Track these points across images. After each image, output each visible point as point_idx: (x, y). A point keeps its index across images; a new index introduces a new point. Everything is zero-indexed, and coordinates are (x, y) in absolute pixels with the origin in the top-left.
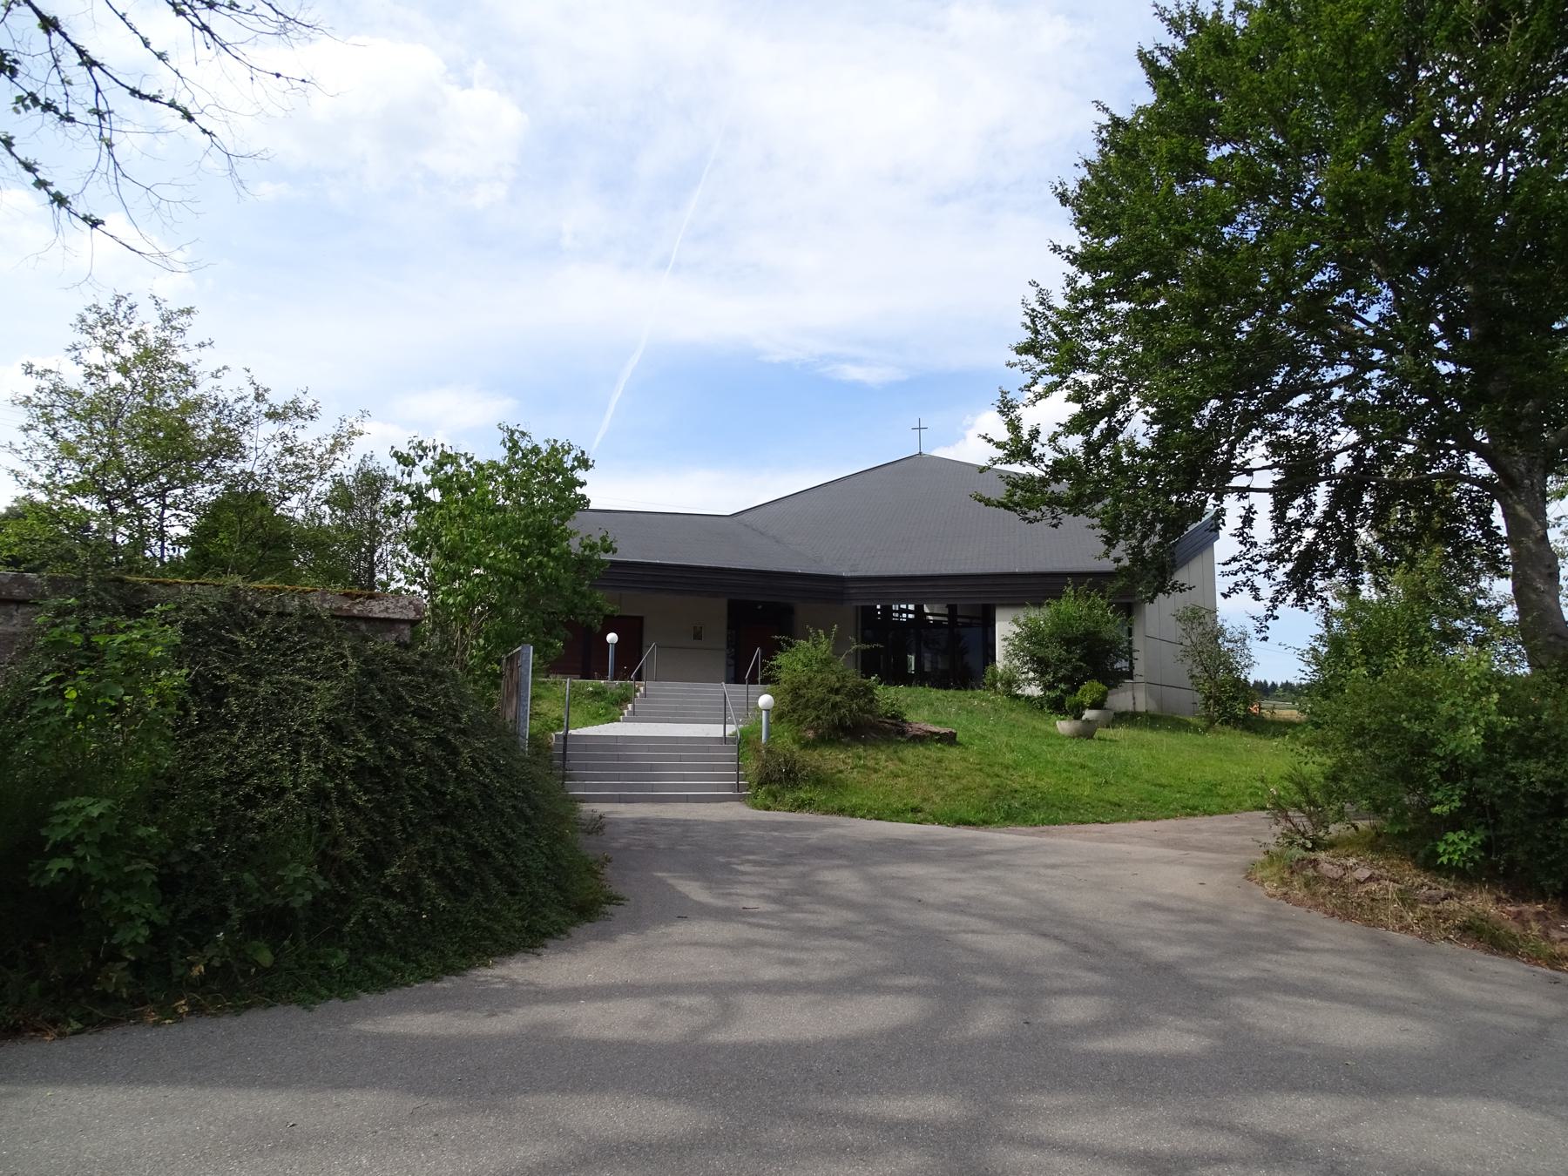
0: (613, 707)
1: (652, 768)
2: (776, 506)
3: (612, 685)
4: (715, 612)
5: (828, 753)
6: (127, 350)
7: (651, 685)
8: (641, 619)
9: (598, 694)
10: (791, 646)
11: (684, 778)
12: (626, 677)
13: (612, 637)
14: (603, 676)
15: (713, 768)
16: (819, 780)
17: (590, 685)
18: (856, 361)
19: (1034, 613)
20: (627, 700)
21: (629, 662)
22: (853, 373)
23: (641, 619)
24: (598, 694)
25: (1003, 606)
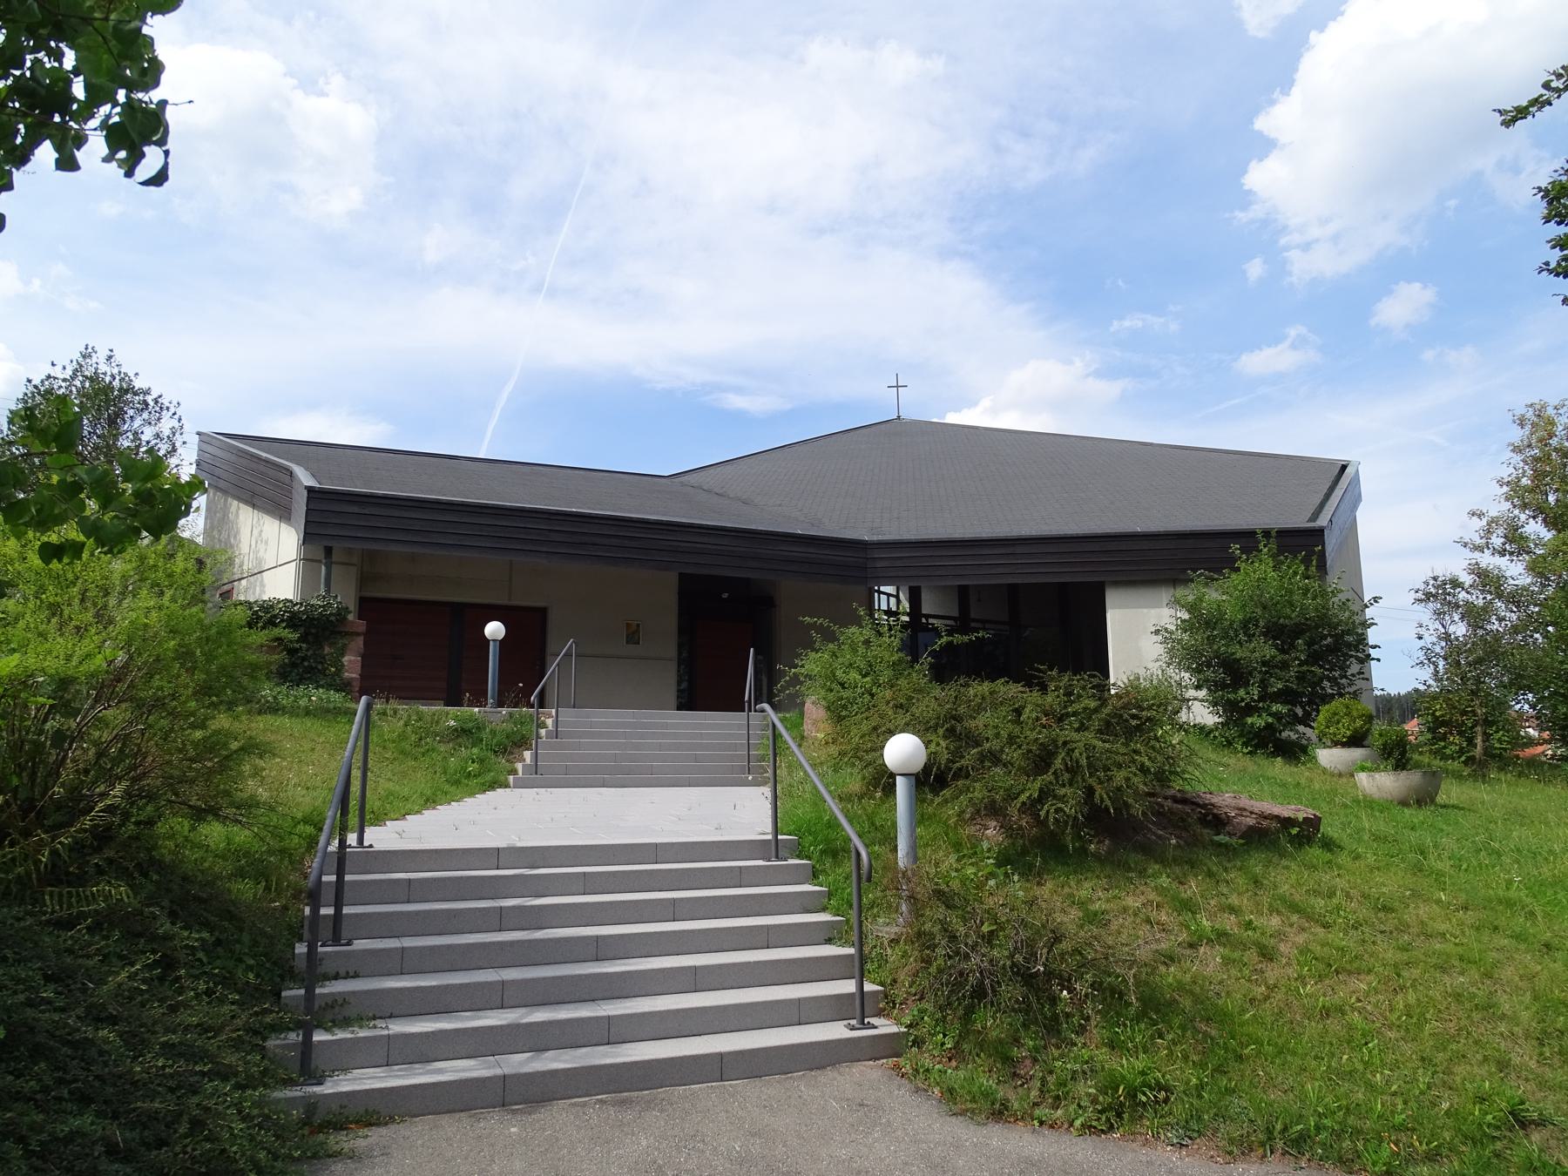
0: (490, 760)
1: (601, 949)
2: (728, 467)
3: (494, 716)
4: (657, 598)
5: (1091, 890)
6: (1280, 1042)
7: (568, 715)
8: (542, 613)
9: (465, 733)
10: (830, 637)
11: (674, 911)
12: (521, 699)
13: (494, 629)
14: (479, 698)
15: (768, 938)
16: (1147, 1006)
17: (451, 717)
18: (739, 390)
19: (1213, 595)
20: (522, 743)
21: (524, 671)
22: (737, 402)
23: (542, 613)
24: (465, 733)
25: (1118, 584)
